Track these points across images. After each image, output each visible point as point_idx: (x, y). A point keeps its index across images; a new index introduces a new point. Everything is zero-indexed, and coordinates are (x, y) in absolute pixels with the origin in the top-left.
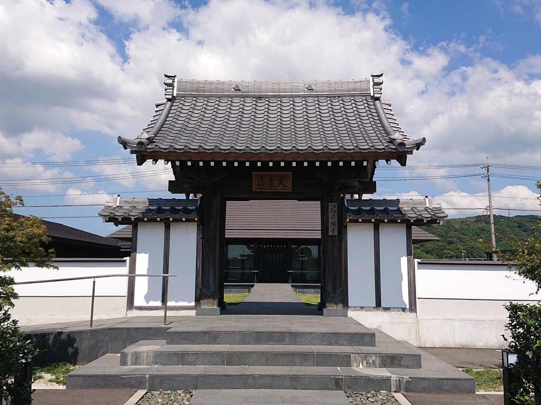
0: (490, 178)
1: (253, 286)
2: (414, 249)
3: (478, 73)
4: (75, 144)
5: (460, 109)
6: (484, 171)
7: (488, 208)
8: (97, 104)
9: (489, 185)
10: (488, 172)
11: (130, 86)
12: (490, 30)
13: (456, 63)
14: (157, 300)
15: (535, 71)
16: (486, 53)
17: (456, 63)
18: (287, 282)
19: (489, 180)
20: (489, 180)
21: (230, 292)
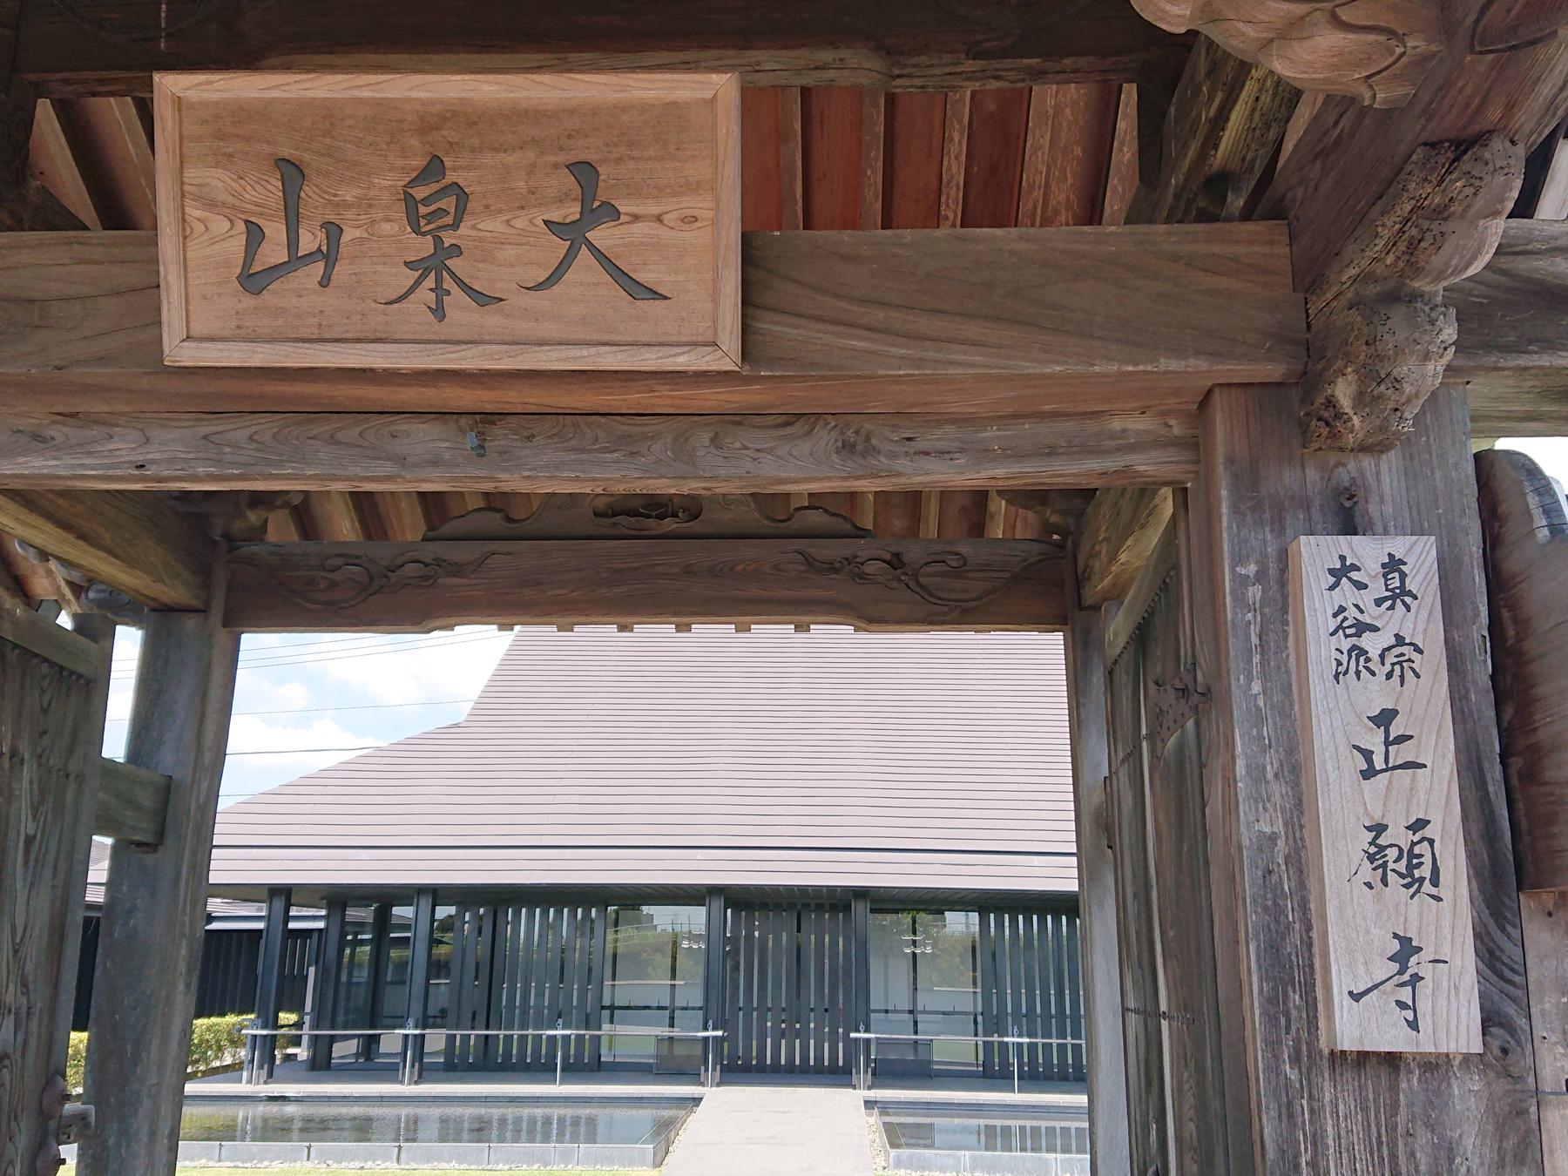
1: (697, 1101)
18: (836, 1074)
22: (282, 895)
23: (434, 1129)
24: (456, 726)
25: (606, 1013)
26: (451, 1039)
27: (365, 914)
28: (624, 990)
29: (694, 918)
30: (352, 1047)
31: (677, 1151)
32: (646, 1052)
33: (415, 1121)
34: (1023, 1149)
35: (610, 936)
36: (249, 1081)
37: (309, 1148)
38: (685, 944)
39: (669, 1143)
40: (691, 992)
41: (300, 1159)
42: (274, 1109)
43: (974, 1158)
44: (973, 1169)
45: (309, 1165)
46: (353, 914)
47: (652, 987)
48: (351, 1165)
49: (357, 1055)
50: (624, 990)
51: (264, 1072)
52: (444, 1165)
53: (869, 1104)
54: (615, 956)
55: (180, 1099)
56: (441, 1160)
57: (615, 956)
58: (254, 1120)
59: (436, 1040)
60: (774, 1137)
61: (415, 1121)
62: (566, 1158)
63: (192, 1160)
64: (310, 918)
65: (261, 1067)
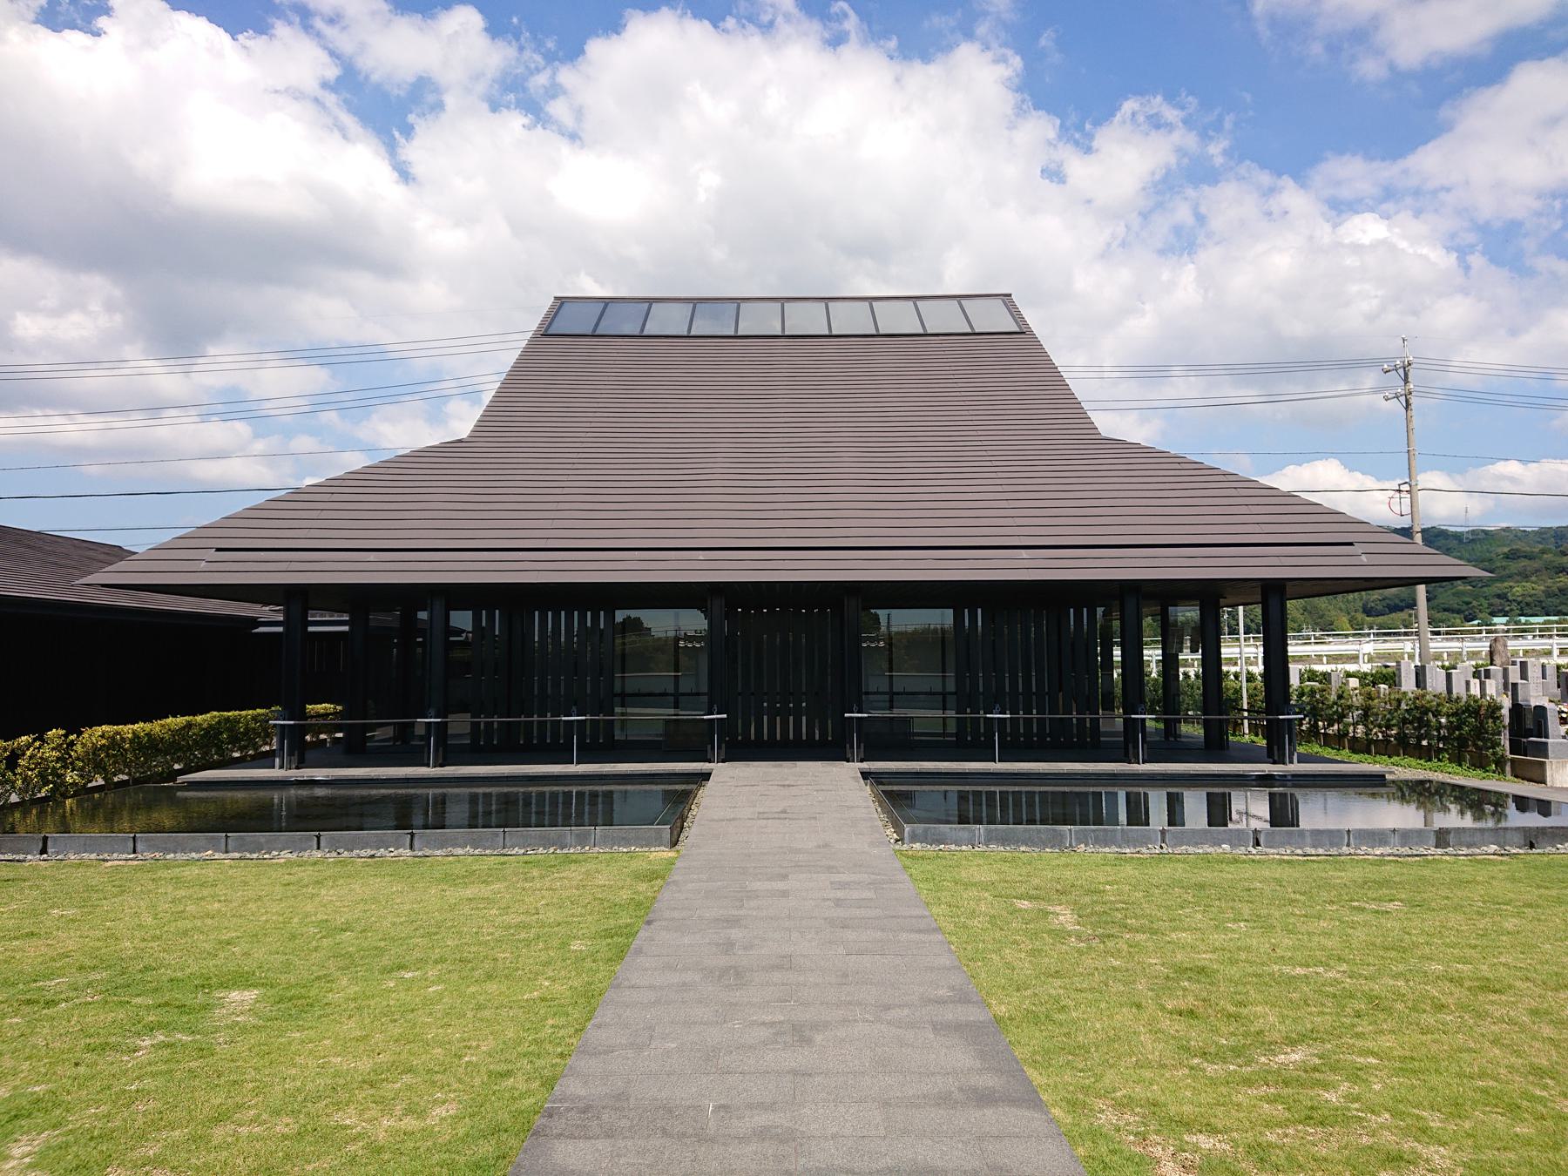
0: (1413, 400)
1: (706, 776)
2: (552, 793)
3: (1230, 203)
4: (312, 378)
5: (1184, 286)
6: (1396, 379)
7: (1406, 487)
8: (364, 282)
9: (1408, 420)
10: (1406, 381)
11: (441, 238)
12: (1248, 98)
13: (1195, 173)
14: (1415, 592)
15: (1345, 193)
16: (1239, 153)
17: (1195, 173)
18: (830, 749)
19: (1408, 406)
20: (1408, 406)
21: (1327, 627)
22: (298, 598)
23: (458, 811)
24: (460, 441)
25: (617, 699)
26: (475, 725)
27: (391, 619)
28: (635, 680)
29: (693, 621)
30: (389, 732)
31: (692, 832)
32: (654, 734)
33: (442, 802)
34: (1031, 821)
35: (618, 641)
36: (281, 767)
37: (318, 837)
38: (682, 644)
39: (683, 819)
40: (696, 679)
41: (311, 848)
42: (304, 792)
43: (988, 832)
44: (987, 842)
45: (319, 854)
46: (377, 618)
47: (660, 678)
48: (363, 853)
49: (395, 739)
50: (635, 680)
51: (295, 758)
52: (460, 851)
53: (865, 775)
54: (623, 656)
55: (860, 640)
56: (455, 845)
57: (623, 656)
58: (288, 804)
59: (460, 724)
60: (784, 812)
61: (442, 802)
62: (582, 841)
63: (198, 851)
64: (327, 623)
65: (290, 754)
